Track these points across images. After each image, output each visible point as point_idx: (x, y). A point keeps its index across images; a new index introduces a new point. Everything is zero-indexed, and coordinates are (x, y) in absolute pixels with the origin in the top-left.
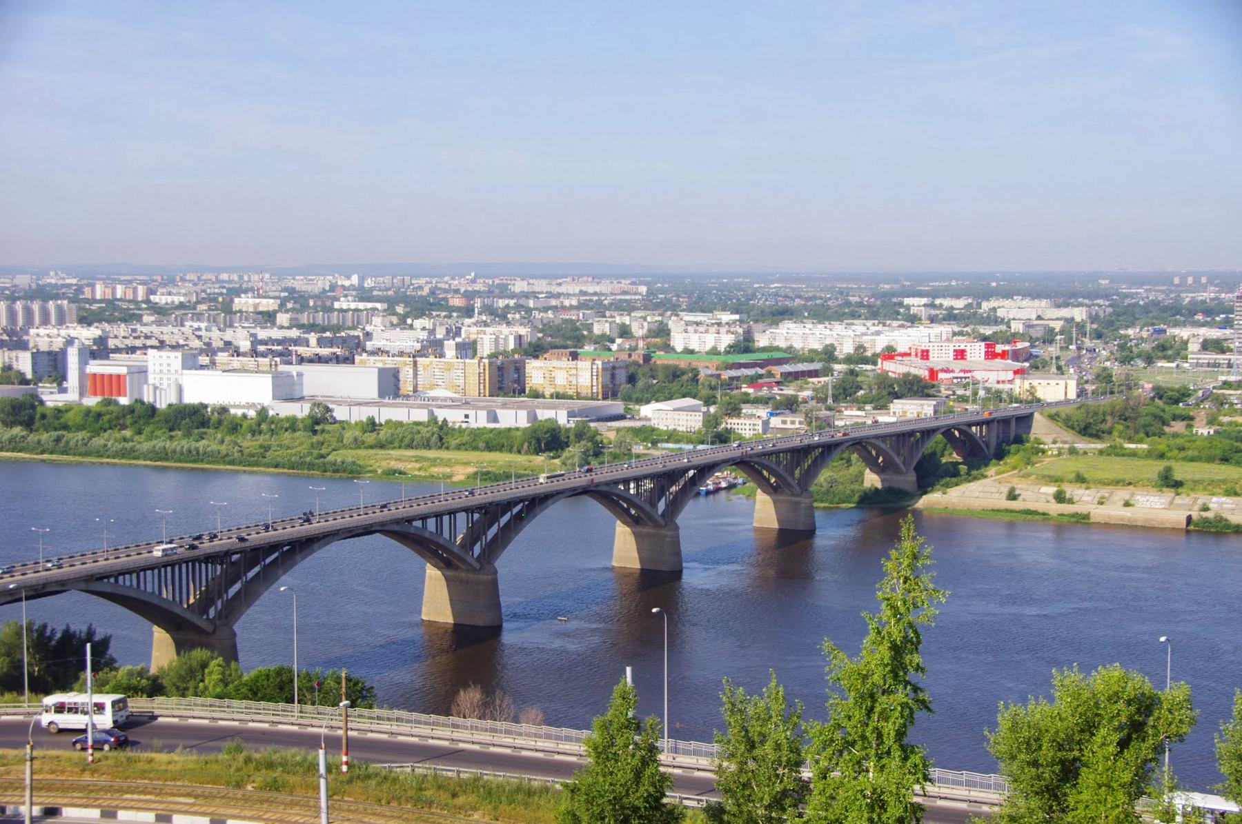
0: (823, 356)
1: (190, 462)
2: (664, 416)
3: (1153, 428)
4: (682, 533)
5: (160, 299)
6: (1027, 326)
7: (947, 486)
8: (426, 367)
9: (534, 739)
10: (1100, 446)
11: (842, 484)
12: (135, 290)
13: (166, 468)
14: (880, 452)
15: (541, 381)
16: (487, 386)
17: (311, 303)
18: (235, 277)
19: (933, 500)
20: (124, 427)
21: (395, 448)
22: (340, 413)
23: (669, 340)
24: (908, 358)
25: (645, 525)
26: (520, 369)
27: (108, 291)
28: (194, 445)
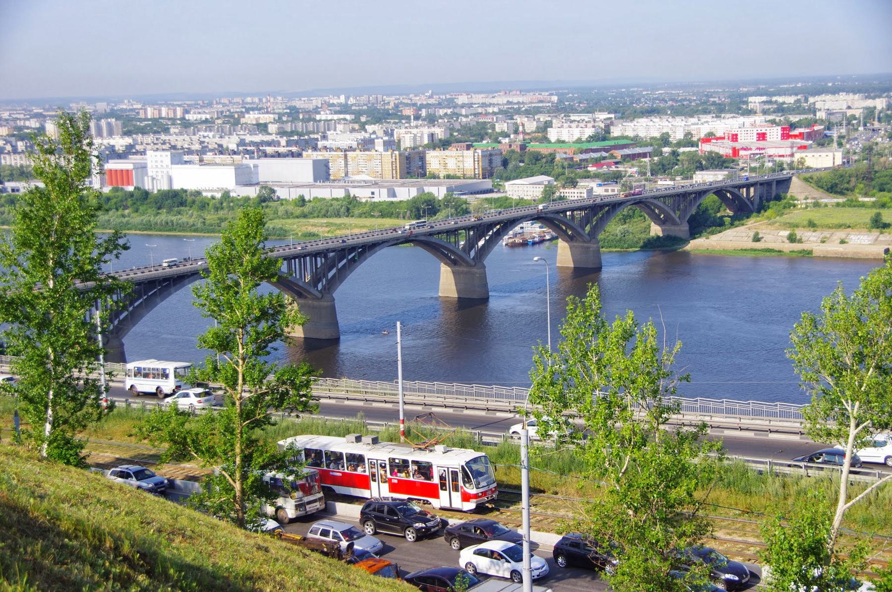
0: (660, 142)
1: (167, 231)
2: (516, 189)
3: (888, 186)
4: (488, 271)
5: (193, 117)
6: (828, 114)
7: (713, 233)
8: (354, 159)
9: (738, 416)
10: (841, 200)
11: (633, 234)
12: (175, 112)
13: (150, 235)
14: (662, 210)
15: (437, 166)
16: (398, 171)
17: (301, 117)
18: (256, 100)
19: (698, 245)
20: (126, 208)
21: (314, 217)
22: (281, 193)
23: (547, 134)
24: (723, 141)
25: (461, 265)
26: (422, 159)
27: (156, 112)
28: (174, 218)
